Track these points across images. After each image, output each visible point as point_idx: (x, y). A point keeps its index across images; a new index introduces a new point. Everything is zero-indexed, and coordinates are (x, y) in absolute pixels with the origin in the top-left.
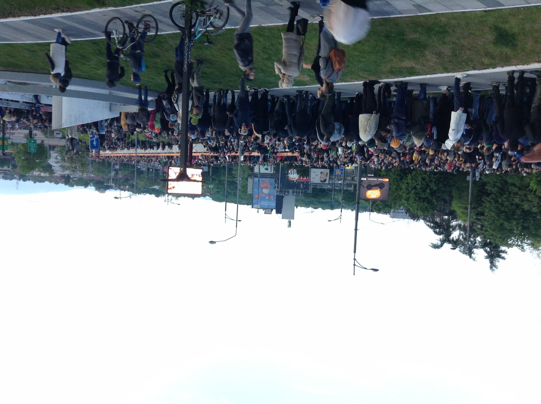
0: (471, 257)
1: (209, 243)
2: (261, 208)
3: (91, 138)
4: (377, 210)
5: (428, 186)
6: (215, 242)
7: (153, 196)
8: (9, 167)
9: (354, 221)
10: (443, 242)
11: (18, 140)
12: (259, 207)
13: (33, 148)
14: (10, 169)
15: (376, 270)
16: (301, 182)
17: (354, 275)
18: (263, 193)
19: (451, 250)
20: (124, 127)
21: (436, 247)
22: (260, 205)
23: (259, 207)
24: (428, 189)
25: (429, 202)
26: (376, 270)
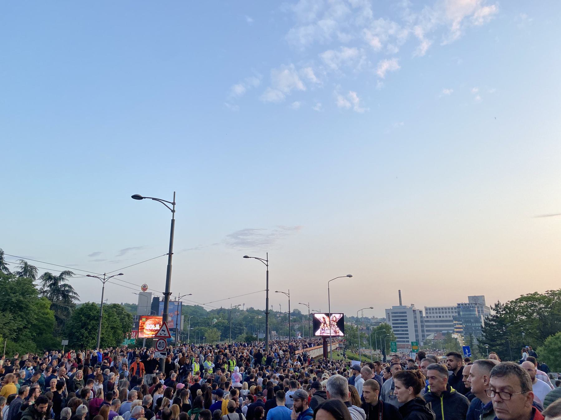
0: (26, 264)
1: (352, 275)
2: (173, 302)
3: (470, 354)
4: (117, 306)
5: (89, 333)
6: (348, 276)
7: (256, 309)
8: (373, 327)
9: (269, 297)
10: (61, 278)
11: (405, 351)
12: (175, 303)
13: (414, 345)
14: (372, 327)
15: (245, 257)
16: (134, 329)
17: (267, 253)
18: (171, 317)
19: (123, 273)
20: (527, 364)
21: (68, 273)
22: (174, 304)
23: (175, 303)
24: (90, 329)
25: (88, 317)
26: (245, 257)
